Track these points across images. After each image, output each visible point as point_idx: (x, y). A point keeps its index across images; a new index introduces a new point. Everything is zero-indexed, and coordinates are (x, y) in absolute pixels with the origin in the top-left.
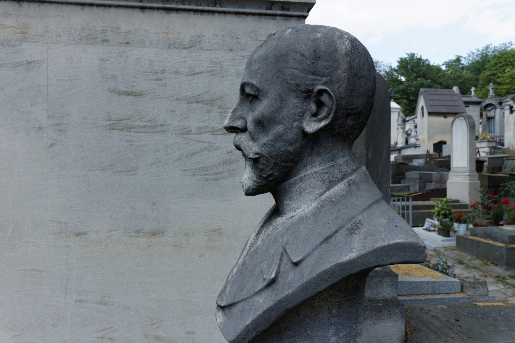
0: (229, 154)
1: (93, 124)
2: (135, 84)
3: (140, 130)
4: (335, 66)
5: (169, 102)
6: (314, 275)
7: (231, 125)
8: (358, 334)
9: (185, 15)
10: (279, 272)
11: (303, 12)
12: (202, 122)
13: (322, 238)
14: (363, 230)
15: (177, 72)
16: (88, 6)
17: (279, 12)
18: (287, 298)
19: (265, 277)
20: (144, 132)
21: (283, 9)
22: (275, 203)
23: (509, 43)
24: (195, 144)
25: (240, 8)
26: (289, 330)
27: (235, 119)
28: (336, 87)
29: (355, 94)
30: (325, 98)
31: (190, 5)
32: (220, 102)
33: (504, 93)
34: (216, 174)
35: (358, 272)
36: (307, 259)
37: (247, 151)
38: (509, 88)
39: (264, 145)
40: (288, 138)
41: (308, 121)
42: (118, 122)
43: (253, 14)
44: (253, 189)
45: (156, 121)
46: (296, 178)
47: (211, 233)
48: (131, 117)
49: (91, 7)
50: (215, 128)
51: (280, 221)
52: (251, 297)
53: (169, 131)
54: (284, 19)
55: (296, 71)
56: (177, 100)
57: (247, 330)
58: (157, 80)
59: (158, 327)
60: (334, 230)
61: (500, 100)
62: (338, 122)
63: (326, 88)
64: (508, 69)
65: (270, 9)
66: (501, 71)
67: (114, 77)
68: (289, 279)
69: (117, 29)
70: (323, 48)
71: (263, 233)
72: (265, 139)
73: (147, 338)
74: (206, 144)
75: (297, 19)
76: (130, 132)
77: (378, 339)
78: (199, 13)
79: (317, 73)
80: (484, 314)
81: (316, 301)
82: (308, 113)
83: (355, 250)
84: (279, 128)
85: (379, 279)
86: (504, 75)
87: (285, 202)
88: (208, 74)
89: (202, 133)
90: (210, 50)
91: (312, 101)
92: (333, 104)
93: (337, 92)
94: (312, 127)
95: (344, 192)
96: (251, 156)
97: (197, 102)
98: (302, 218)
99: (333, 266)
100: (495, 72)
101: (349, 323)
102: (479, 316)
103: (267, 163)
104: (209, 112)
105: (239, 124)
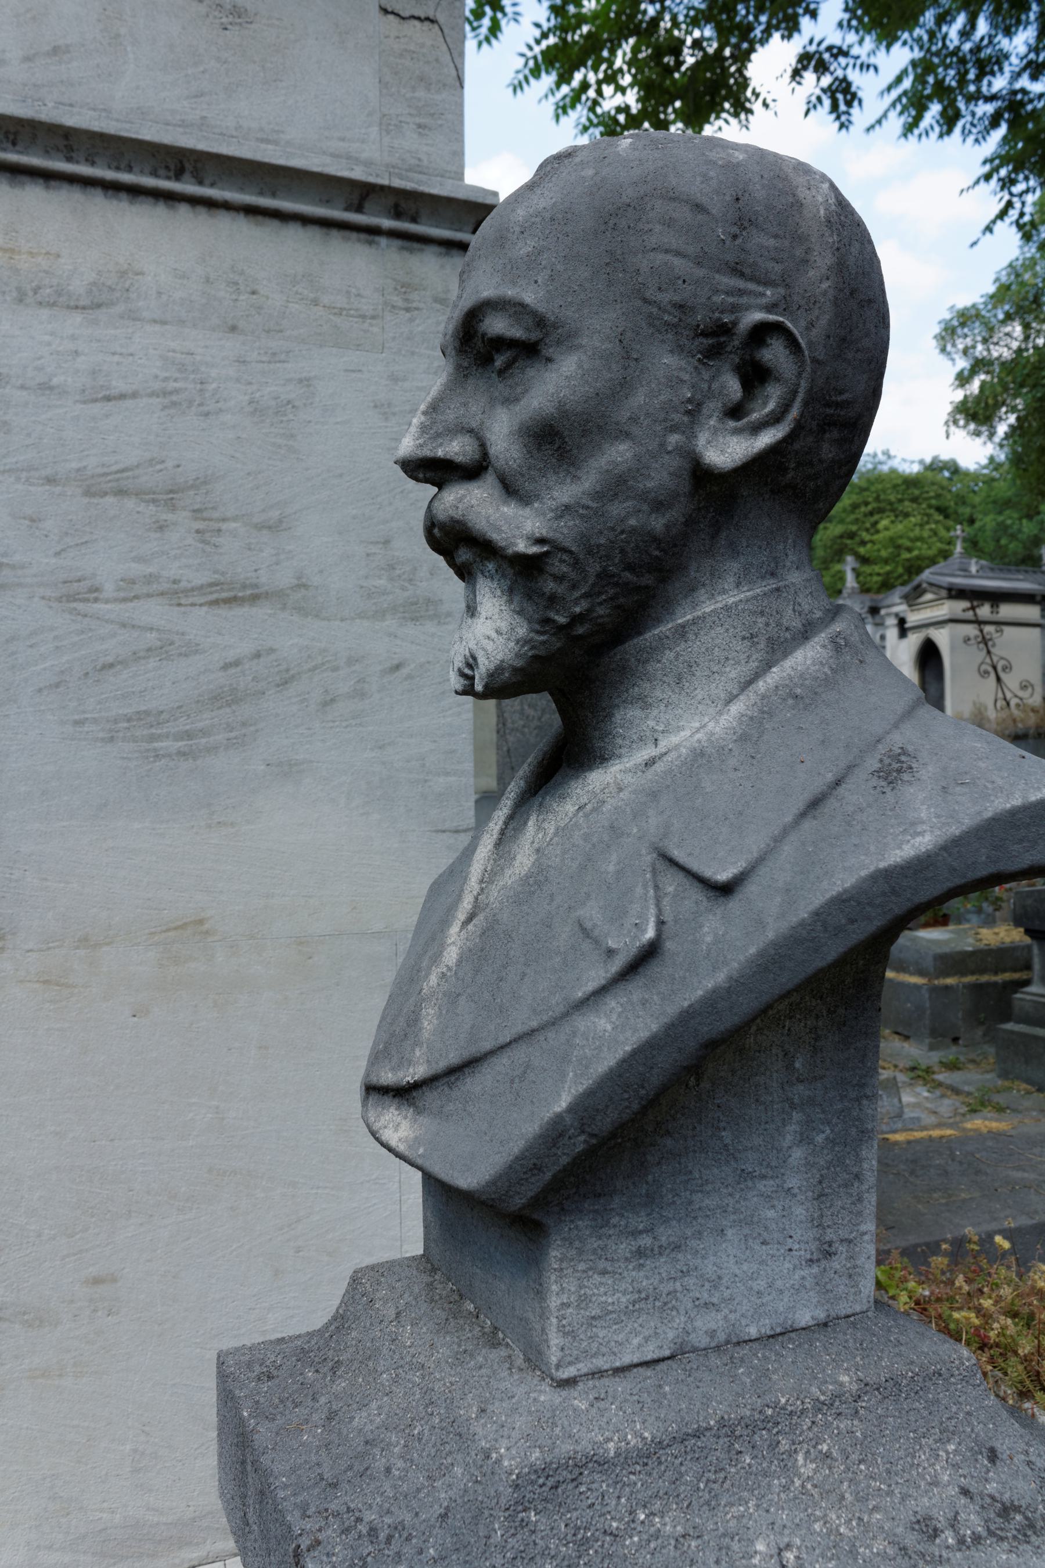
0: (232, 671)
5: (20, 487)
6: (803, 912)
7: (427, 452)
9: (75, 196)
11: (460, 230)
12: (138, 559)
14: (928, 771)
15: (46, 387)
17: (387, 223)
18: (711, 1002)
21: (398, 215)
23: (884, 453)
25: (261, 193)
27: (438, 435)
30: (775, 353)
31: (93, 164)
32: (198, 499)
33: (875, 586)
34: (189, 735)
36: (762, 870)
37: (499, 530)
38: (888, 573)
39: (567, 509)
40: (650, 484)
41: (715, 431)
43: (305, 220)
44: (515, 670)
47: (171, 934)
50: (184, 584)
54: (403, 248)
55: (677, 262)
56: (50, 480)
57: (555, 1133)
60: (830, 777)
61: (872, 600)
63: (781, 319)
64: (884, 523)
65: (359, 209)
66: (868, 525)
72: (565, 492)
75: (443, 250)
78: (123, 195)
79: (747, 271)
80: (914, 1161)
82: (713, 408)
84: (618, 454)
86: (875, 537)
87: (618, 717)
88: (155, 401)
89: (136, 597)
90: (164, 323)
91: (727, 366)
92: (800, 374)
94: (727, 450)
96: (522, 546)
97: (121, 492)
98: (702, 754)
99: (864, 880)
100: (854, 528)
102: (902, 1167)
103: (573, 575)
104: (161, 528)
105: (457, 449)
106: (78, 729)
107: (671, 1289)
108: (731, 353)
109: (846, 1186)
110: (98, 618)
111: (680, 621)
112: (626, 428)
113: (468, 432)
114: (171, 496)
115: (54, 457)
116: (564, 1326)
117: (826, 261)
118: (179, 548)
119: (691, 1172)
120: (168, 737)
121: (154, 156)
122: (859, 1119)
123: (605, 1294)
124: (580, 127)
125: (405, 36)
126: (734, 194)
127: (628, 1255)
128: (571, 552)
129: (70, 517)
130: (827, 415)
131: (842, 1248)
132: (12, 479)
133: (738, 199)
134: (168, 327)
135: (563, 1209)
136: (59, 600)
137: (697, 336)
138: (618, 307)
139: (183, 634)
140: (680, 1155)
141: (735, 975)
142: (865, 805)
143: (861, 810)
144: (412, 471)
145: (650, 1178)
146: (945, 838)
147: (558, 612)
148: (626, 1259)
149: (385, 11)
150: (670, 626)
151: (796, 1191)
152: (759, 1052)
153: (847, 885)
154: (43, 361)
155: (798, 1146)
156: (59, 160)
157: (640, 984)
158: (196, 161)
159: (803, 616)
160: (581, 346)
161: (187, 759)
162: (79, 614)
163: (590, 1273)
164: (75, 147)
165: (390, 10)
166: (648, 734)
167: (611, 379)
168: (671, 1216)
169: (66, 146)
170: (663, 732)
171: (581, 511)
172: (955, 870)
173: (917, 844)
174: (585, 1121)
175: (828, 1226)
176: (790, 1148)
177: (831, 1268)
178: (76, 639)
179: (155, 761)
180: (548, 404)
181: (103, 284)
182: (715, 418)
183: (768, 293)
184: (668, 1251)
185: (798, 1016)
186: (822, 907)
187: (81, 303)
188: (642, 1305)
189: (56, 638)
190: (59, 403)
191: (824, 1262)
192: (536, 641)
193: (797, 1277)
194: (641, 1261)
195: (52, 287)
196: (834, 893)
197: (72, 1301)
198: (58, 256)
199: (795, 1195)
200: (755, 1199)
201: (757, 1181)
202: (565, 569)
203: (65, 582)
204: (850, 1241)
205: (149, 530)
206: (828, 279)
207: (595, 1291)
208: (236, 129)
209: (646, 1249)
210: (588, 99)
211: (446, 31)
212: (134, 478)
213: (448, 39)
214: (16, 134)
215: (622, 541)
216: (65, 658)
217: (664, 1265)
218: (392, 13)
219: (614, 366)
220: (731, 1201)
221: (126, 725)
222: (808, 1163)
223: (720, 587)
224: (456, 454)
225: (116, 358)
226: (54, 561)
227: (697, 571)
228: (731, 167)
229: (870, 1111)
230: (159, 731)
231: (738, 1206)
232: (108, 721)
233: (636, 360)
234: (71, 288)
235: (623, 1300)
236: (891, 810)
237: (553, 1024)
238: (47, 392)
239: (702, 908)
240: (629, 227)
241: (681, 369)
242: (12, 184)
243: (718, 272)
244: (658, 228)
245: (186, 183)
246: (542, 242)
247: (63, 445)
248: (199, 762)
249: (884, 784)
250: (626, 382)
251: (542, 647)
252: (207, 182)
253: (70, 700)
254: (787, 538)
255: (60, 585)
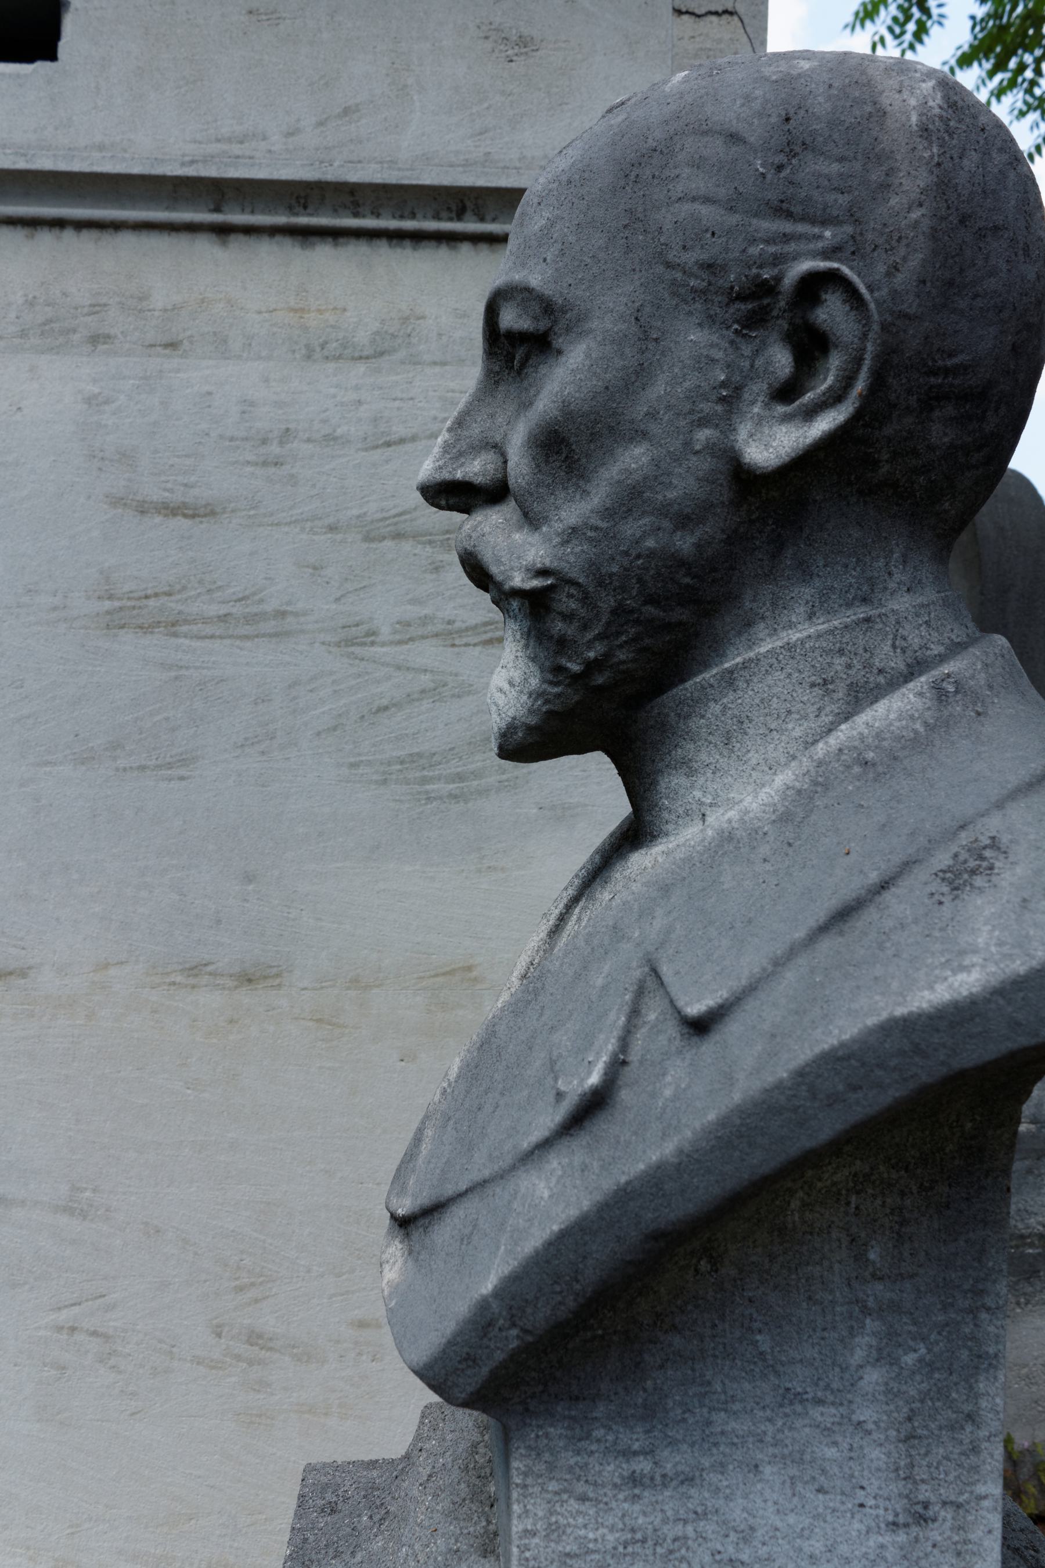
1: (55, 609)
2: (193, 479)
3: (209, 630)
4: (874, 177)
5: (304, 536)
6: (781, 1071)
7: (446, 475)
8: (984, 1361)
9: (360, 249)
10: (624, 1063)
12: (414, 601)
13: (820, 912)
14: (1011, 875)
15: (331, 439)
16: (46, 229)
18: (656, 1180)
19: (561, 1085)
20: (221, 637)
22: (630, 809)
24: (389, 678)
26: (674, 1327)
28: (881, 269)
29: (962, 304)
30: (832, 313)
34: (460, 777)
35: (996, 1063)
36: (750, 1005)
37: (499, 561)
39: (574, 532)
40: (671, 495)
41: (759, 421)
42: (138, 603)
44: (529, 729)
45: (261, 601)
46: (706, 675)
47: (440, 979)
48: (178, 587)
49: (56, 231)
50: (458, 625)
51: (641, 861)
52: (502, 1176)
53: (302, 631)
56: (332, 529)
58: (265, 464)
59: (256, 1301)
60: (874, 877)
62: (888, 430)
63: (835, 265)
67: (126, 457)
68: (668, 1092)
69: (141, 299)
70: (821, 105)
71: (574, 918)
72: (573, 511)
73: (219, 1335)
74: (425, 679)
76: (175, 635)
77: (1025, 1371)
78: (407, 243)
79: (797, 209)
81: (795, 1204)
82: (758, 389)
83: (976, 959)
85: (1027, 1163)
87: (662, 786)
89: (411, 639)
90: (444, 364)
91: (775, 336)
92: (864, 336)
93: (884, 292)
94: (771, 442)
95: (918, 726)
96: (518, 580)
97: (398, 536)
98: (730, 838)
99: (871, 1031)
101: (945, 1308)
103: (583, 612)
105: (476, 469)
106: (353, 771)
107: (680, 1534)
108: (778, 317)
109: (952, 1428)
110: (375, 662)
111: (727, 665)
112: (643, 427)
113: (493, 447)
114: (448, 536)
115: (337, 505)
116: (527, 1560)
117: (918, 182)
118: (454, 588)
119: (709, 1383)
120: (439, 779)
121: (435, 199)
122: (973, 1338)
123: (585, 1526)
124: (1016, 112)
125: (701, 35)
126: (783, 113)
127: (618, 1481)
128: (577, 584)
129: (349, 564)
130: (932, 387)
131: (947, 1514)
132: (297, 530)
133: (788, 119)
134: (447, 368)
135: (527, 1410)
136: (338, 644)
137: (732, 301)
138: (636, 277)
139: (456, 675)
140: (693, 1359)
141: (687, 1148)
142: (910, 920)
143: (903, 926)
144: (432, 497)
145: (649, 1384)
146: (1001, 977)
147: (570, 659)
148: (615, 1485)
149: (679, 12)
150: (714, 671)
151: (870, 1426)
152: (811, 1234)
153: (846, 1037)
154: (328, 413)
155: (874, 1366)
156: (347, 217)
157: (584, 1143)
158: (477, 198)
159: (909, 653)
160: (591, 331)
161: (458, 802)
162: (356, 658)
163: (565, 1497)
164: (361, 202)
165: (684, 10)
166: (694, 807)
167: (624, 368)
168: (680, 1437)
169: (352, 202)
170: (711, 805)
171: (589, 534)
172: (1018, 1024)
173: (956, 984)
174: (514, 1312)
175: (923, 1481)
176: (861, 1367)
177: (927, 1539)
178: (354, 682)
179: (426, 804)
180: (552, 405)
181: (386, 332)
182: (759, 404)
183: (828, 234)
184: (674, 1483)
185: (870, 1191)
186: (807, 1065)
187: (365, 353)
188: (638, 1548)
189: (334, 682)
190: (342, 452)
191: (915, 1530)
192: (550, 693)
193: (871, 1543)
194: (637, 1491)
195: (337, 341)
196: (826, 1047)
197: (338, 1342)
198: (345, 310)
199: (869, 1433)
200: (807, 1430)
201: (809, 1406)
202: (573, 605)
203: (344, 627)
204: (959, 1506)
205: (425, 572)
206: (921, 205)
207: (571, 1520)
208: (520, 160)
209: (643, 1476)
210: (1024, 80)
211: (746, 21)
212: (412, 520)
213: (748, 29)
214: (306, 197)
215: (639, 568)
216: (342, 702)
217: (669, 1501)
218: (687, 12)
219: (627, 351)
220: (770, 1429)
221: (399, 767)
222: (888, 1391)
223: (785, 619)
224: (475, 474)
225: (397, 404)
226: (334, 606)
227: (754, 601)
228: (789, 80)
229: (991, 1329)
230: (431, 774)
231: (780, 1436)
232: (382, 764)
233: (656, 340)
234: (355, 339)
235: (610, 1537)
236: (941, 930)
237: (502, 1177)
238: (332, 443)
239: (673, 1049)
240: (653, 177)
241: (712, 346)
242: (303, 246)
243: (756, 215)
244: (687, 171)
245: (468, 221)
246: (556, 212)
247: (345, 493)
248: (470, 805)
249: (945, 889)
250: (643, 370)
251: (557, 701)
252: (488, 217)
253: (346, 743)
254: (891, 552)
255: (340, 630)
